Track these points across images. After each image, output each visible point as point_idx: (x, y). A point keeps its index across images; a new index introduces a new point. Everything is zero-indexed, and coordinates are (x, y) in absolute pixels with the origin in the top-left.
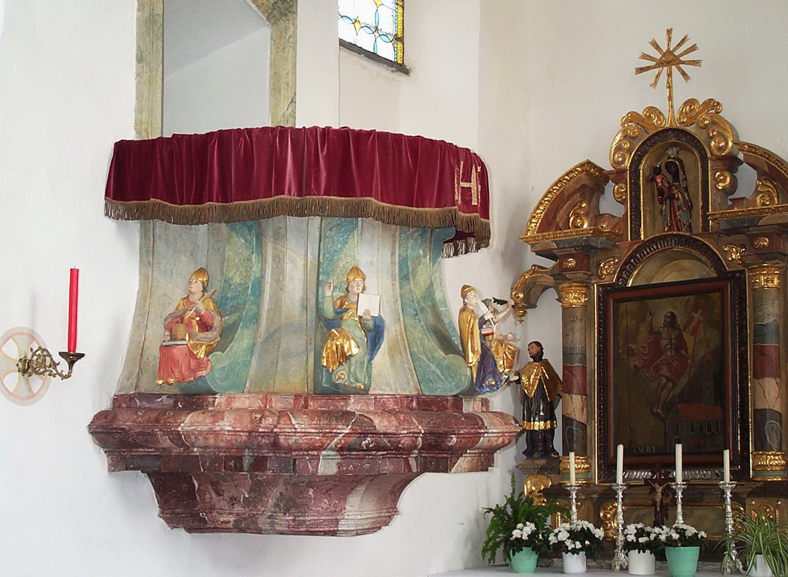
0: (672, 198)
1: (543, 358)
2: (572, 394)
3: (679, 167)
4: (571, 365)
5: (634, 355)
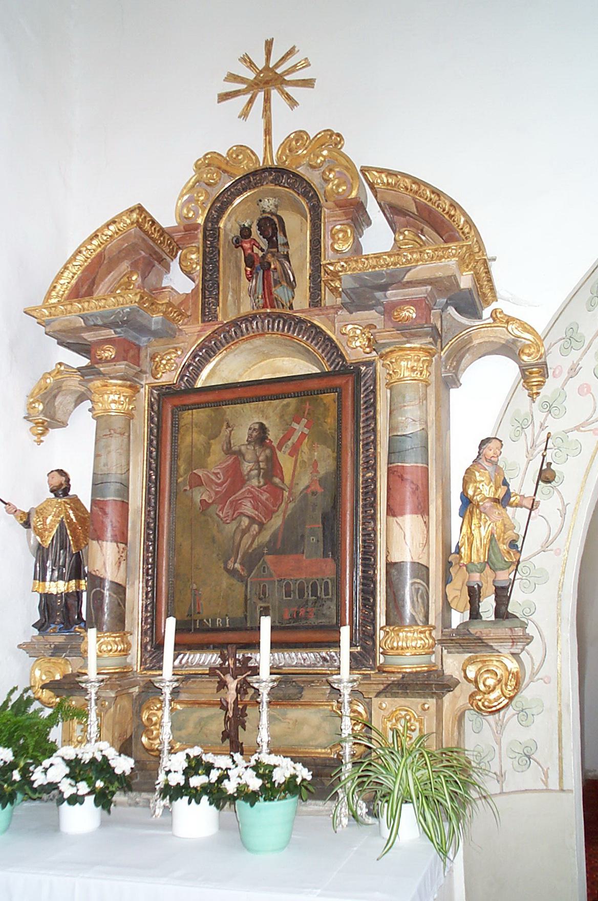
0: (266, 267)
1: (70, 493)
2: (103, 541)
3: (277, 226)
4: (102, 499)
5: (201, 484)
